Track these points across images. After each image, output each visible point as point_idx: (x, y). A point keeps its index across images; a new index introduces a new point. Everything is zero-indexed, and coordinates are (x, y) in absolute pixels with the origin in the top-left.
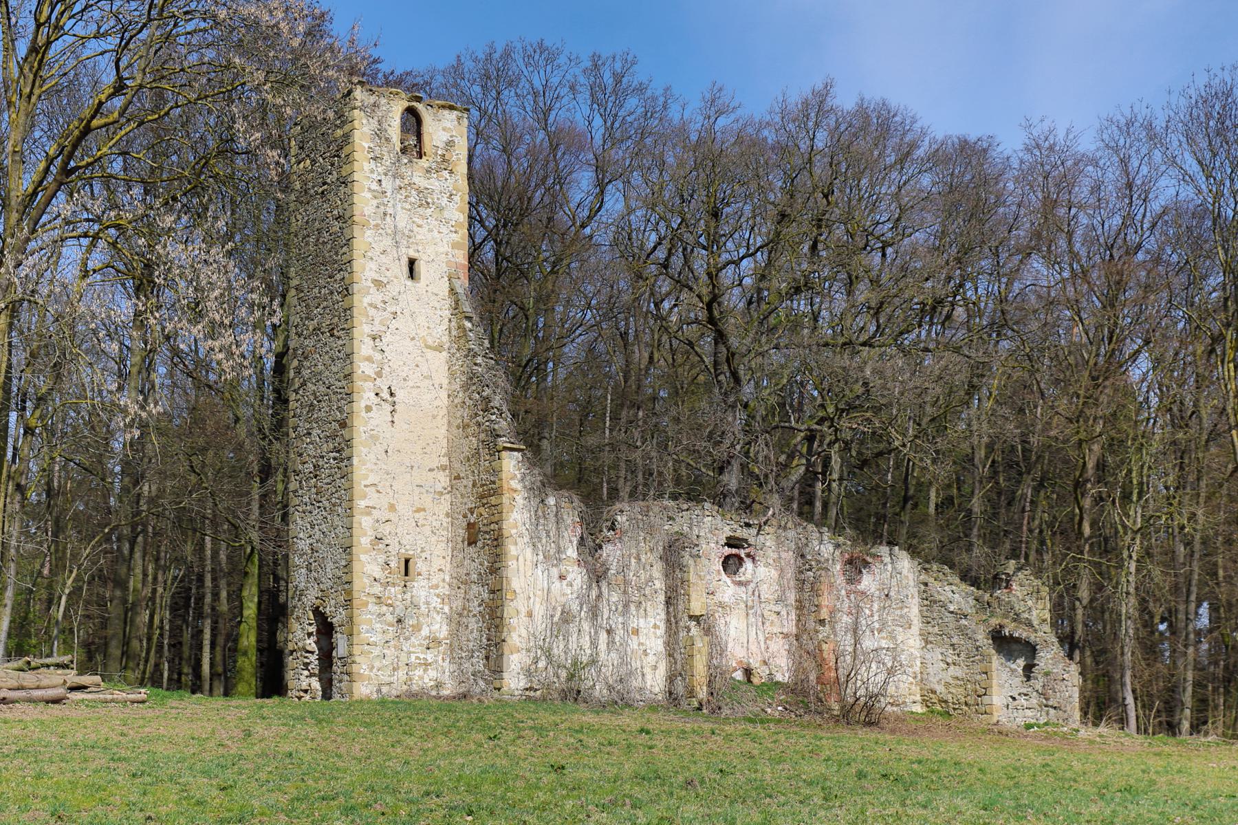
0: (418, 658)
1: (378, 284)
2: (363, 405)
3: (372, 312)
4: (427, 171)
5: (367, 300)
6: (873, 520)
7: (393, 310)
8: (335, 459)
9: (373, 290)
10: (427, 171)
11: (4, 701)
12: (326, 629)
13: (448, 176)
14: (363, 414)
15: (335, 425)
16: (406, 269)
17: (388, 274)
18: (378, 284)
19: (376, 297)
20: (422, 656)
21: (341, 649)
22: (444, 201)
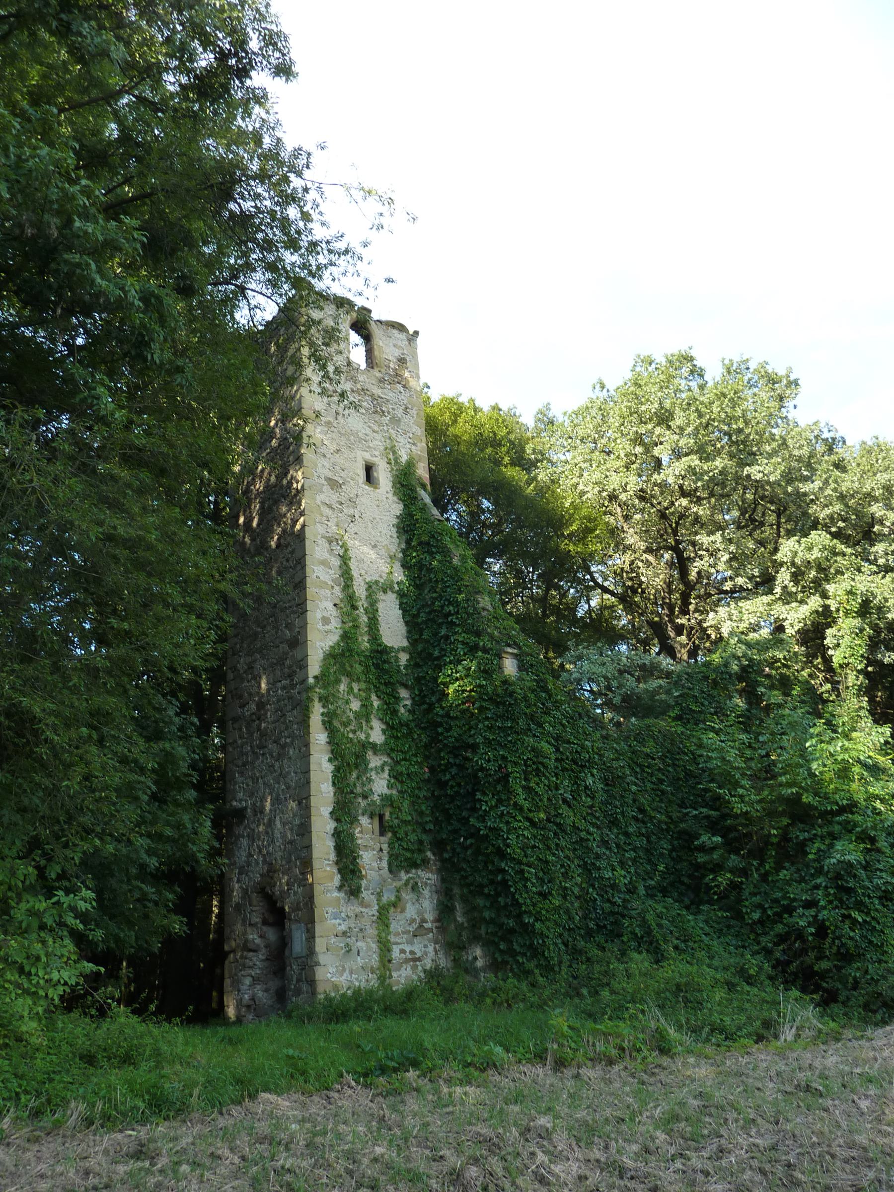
0: (403, 951)
1: (334, 485)
2: (319, 615)
3: (326, 511)
4: (380, 381)
5: (320, 498)
6: (707, 1029)
7: (351, 511)
8: (284, 688)
9: (326, 488)
10: (380, 381)
11: (1, 1176)
12: (277, 917)
13: (402, 390)
14: (320, 626)
15: (285, 647)
16: (362, 473)
17: (343, 474)
18: (334, 485)
19: (327, 495)
20: (408, 949)
21: (298, 945)
22: (399, 412)
